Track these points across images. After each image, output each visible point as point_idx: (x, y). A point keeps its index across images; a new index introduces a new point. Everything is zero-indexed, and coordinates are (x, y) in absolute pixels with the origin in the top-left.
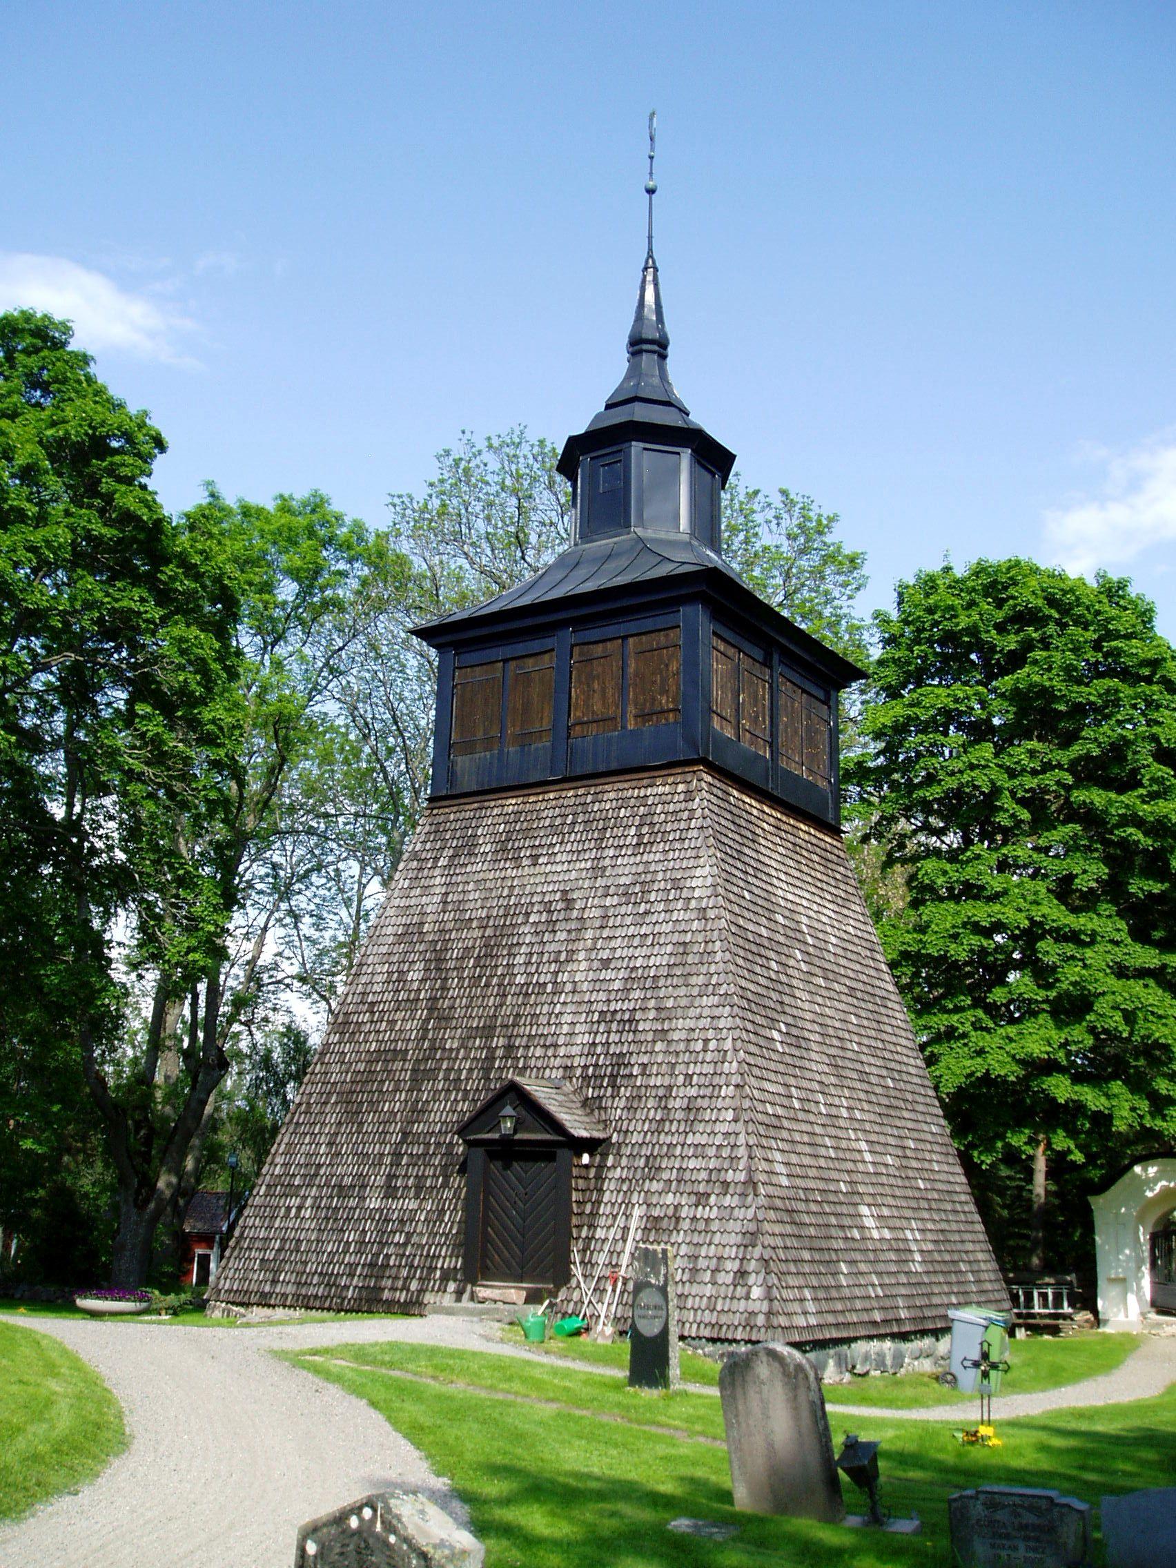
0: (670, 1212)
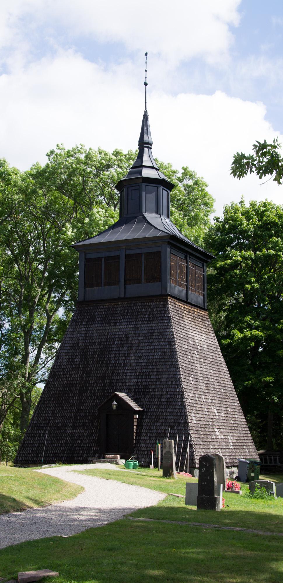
0: (163, 431)
